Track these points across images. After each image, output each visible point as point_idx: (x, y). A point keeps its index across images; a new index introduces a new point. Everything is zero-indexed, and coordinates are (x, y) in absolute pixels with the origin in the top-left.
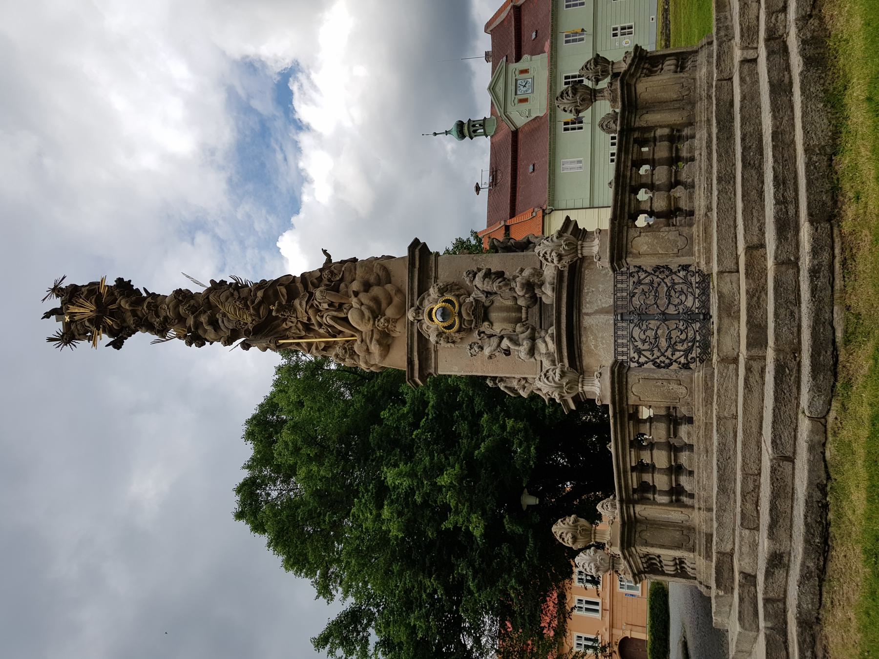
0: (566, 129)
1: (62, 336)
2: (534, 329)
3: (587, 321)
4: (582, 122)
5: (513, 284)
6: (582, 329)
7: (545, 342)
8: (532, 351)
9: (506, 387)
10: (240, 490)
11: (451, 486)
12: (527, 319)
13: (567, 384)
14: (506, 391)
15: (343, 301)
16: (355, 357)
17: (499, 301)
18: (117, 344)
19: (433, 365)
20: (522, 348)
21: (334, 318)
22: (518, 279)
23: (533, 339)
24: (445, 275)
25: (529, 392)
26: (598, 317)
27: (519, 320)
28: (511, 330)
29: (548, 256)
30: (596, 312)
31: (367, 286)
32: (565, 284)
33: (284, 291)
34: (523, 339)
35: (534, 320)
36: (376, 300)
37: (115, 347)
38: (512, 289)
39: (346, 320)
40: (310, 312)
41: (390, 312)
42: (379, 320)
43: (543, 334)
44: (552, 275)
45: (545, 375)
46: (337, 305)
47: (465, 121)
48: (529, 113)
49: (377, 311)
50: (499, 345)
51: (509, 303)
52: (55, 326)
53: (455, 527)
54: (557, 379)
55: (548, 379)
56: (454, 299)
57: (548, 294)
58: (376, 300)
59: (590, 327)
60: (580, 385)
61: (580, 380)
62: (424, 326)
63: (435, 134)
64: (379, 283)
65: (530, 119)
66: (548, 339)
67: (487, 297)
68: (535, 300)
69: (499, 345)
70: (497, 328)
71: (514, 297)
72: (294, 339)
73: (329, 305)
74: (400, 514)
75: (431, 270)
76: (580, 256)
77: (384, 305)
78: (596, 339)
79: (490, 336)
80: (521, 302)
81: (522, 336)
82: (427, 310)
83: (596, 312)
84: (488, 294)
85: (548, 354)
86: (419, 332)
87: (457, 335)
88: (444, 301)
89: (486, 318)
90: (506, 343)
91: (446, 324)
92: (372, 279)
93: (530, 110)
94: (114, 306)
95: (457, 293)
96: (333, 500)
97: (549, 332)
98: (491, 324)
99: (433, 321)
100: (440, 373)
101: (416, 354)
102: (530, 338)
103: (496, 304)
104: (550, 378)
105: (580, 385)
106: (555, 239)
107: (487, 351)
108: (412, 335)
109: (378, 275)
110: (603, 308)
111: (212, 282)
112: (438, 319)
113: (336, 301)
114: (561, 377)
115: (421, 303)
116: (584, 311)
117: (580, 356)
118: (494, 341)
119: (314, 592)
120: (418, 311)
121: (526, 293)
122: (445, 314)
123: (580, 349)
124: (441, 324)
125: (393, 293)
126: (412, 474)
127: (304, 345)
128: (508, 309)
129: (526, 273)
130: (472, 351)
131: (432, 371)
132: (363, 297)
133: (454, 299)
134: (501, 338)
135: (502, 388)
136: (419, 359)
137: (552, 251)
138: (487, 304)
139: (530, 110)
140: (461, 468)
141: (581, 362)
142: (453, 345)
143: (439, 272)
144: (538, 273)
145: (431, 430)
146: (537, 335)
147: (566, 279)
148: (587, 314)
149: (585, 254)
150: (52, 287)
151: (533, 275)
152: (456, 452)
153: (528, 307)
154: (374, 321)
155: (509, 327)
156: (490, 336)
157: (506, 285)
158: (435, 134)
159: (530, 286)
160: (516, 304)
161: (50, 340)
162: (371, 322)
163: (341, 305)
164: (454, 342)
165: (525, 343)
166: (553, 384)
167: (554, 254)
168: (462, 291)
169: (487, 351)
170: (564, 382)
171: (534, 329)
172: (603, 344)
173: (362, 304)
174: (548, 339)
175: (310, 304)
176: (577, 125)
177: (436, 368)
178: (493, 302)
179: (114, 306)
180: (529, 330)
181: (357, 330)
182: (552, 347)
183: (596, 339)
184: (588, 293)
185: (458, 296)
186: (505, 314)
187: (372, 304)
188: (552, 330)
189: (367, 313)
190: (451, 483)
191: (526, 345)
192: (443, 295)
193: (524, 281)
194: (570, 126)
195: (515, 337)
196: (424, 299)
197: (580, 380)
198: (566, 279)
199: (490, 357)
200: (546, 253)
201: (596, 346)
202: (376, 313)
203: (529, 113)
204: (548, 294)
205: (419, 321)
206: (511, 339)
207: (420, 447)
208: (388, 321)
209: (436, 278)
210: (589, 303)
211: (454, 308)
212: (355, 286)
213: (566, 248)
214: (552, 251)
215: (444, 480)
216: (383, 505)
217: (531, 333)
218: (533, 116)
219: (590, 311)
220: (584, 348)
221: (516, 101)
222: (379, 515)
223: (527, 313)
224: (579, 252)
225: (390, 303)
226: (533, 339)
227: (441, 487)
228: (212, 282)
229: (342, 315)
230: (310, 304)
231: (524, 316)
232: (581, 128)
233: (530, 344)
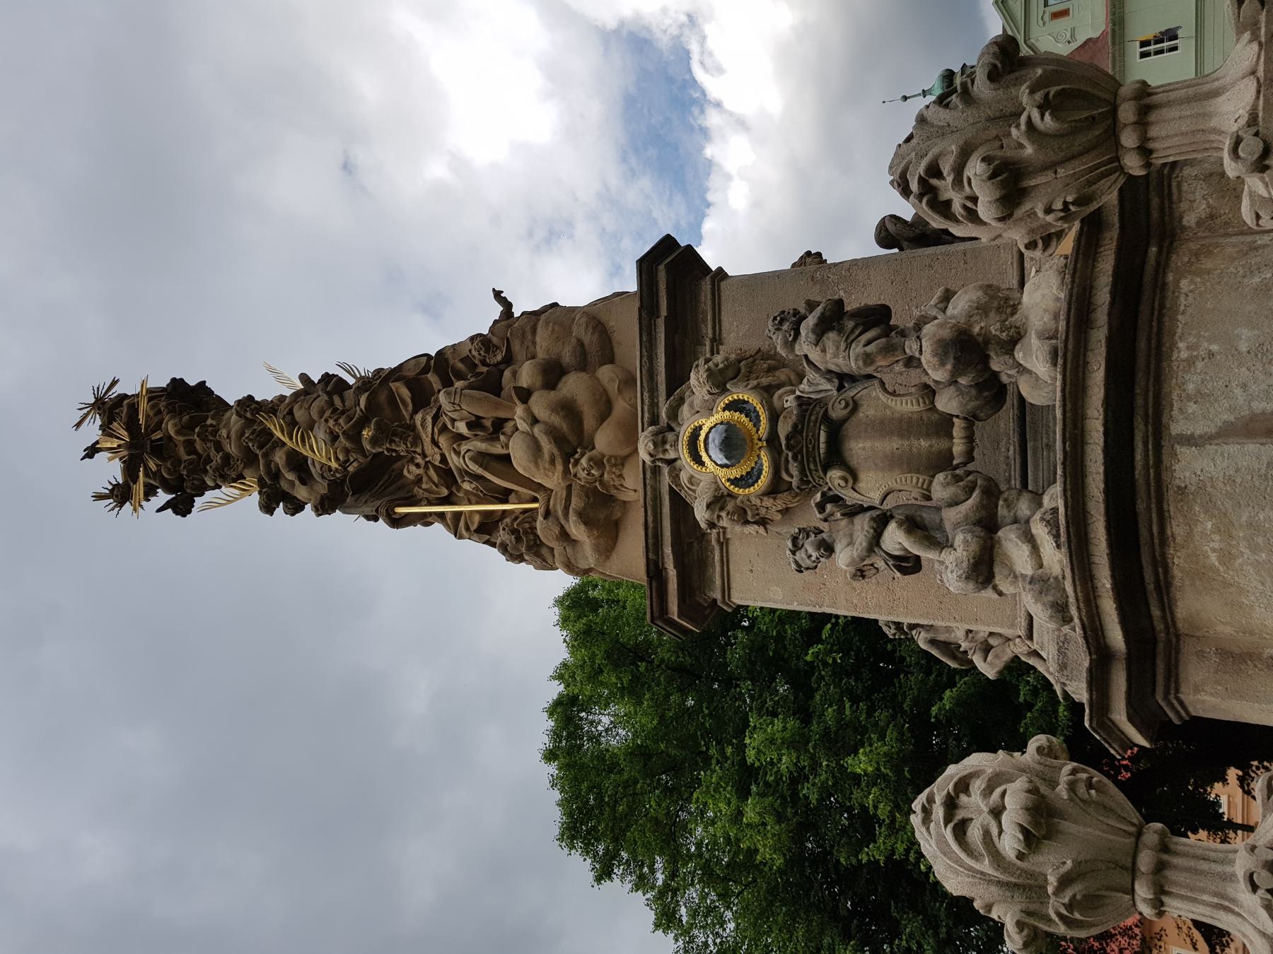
0: (1144, 55)
1: (112, 491)
2: (992, 493)
3: (1189, 466)
4: (1176, 38)
5: (911, 347)
6: (1170, 495)
7: (1030, 539)
8: (983, 569)
9: (933, 642)
10: (552, 711)
11: (876, 778)
12: (969, 457)
13: (1065, 882)
14: (935, 652)
15: (502, 415)
16: (544, 551)
17: (874, 403)
18: (182, 506)
19: (718, 582)
20: (948, 557)
21: (481, 458)
22: (928, 329)
23: (987, 525)
24: (740, 332)
25: (1000, 665)
26: (1232, 448)
27: (942, 462)
28: (916, 493)
29: (947, 191)
30: (1227, 433)
31: (553, 374)
32: (1099, 335)
33: (405, 393)
34: (956, 526)
35: (998, 455)
36: (569, 409)
37: (176, 513)
38: (912, 362)
39: (506, 459)
40: (443, 441)
41: (604, 440)
42: (577, 462)
43: (1023, 507)
44: (1051, 305)
45: (951, 804)
46: (488, 423)
47: (957, 69)
48: (1073, 36)
49: (572, 438)
50: (875, 542)
51: (908, 406)
52: (109, 469)
53: (889, 858)
54: (1009, 844)
55: (960, 831)
56: (754, 400)
57: (1036, 373)
58: (569, 409)
59: (1201, 487)
60: (1143, 891)
61: (1145, 861)
62: (684, 477)
63: (905, 98)
64: (583, 364)
65: (1075, 45)
66: (1040, 531)
67: (840, 388)
68: (993, 392)
69: (875, 542)
70: (872, 488)
71: (926, 386)
72: (430, 504)
73: (470, 426)
74: (780, 818)
75: (704, 320)
76: (1133, 164)
77: (589, 421)
78: (1225, 530)
79: (853, 512)
80: (947, 403)
81: (951, 516)
82: (685, 432)
83: (1227, 433)
84: (843, 379)
85: (1041, 583)
86: (672, 492)
87: (768, 502)
88: (728, 407)
89: (836, 456)
90: (895, 539)
91: (735, 473)
92: (567, 358)
93: (1073, 30)
94: (157, 435)
95: (765, 381)
96: (670, 762)
97: (1047, 502)
98: (853, 475)
99: (702, 464)
100: (737, 599)
101: (668, 550)
102: (978, 523)
103: (868, 411)
104: (974, 833)
105: (1143, 891)
106: (982, 87)
107: (843, 557)
108: (657, 499)
109: (581, 343)
110: (1254, 418)
111: (304, 378)
112: (714, 456)
113: (488, 414)
114: (1032, 839)
115: (674, 414)
116: (1178, 427)
117: (1165, 587)
118: (862, 525)
119: (651, 916)
120: (663, 436)
121: (956, 373)
122: (733, 444)
123: (1162, 565)
124: (721, 473)
125: (613, 388)
126: (797, 743)
127: (448, 517)
128: (903, 427)
129: (960, 306)
130: (800, 555)
131: (717, 595)
132: (540, 404)
133: (754, 400)
134: (882, 521)
135: (923, 646)
136: (678, 564)
137: (965, 154)
138: (837, 412)
139: (1073, 30)
140: (901, 739)
141: (1167, 605)
142: (761, 530)
143: (725, 325)
144: (1002, 302)
145: (845, 649)
146: (1002, 511)
147: (1101, 317)
148: (1189, 440)
149: (1165, 152)
150: (92, 400)
151: (982, 309)
152: (895, 695)
153: (971, 420)
154: (566, 463)
155: (907, 489)
156: (853, 512)
157: (889, 350)
158: (905, 98)
159: (968, 350)
160: (933, 409)
161: (99, 497)
162: (560, 467)
163: (499, 424)
164: (763, 522)
165: (959, 539)
166: (985, 866)
167: (975, 168)
168: (782, 375)
169: (843, 557)
170: (1052, 865)
171: (992, 493)
172: (1255, 549)
173: (535, 421)
174: (1040, 531)
175: (439, 425)
176: (1166, 45)
177: (726, 588)
178: (854, 406)
179: (157, 435)
180: (976, 493)
181: (540, 487)
182: (1055, 559)
183: (1225, 530)
184: (1191, 362)
185: (767, 391)
186: (893, 444)
187: (556, 420)
188: (1054, 497)
189: (547, 445)
190: (878, 769)
191: (962, 547)
192: (724, 390)
193: (946, 333)
194: (1152, 48)
195: (928, 517)
196: (681, 400)
197: (1145, 861)
198: (1101, 317)
199: (860, 574)
200: (934, 170)
201: (1227, 557)
202: (570, 442)
203: (1073, 36)
204: (1036, 373)
205: (671, 462)
206: (913, 525)
207: (823, 677)
208: (598, 463)
209: (717, 341)
210: (1199, 397)
211: (757, 424)
212: (526, 374)
213: (1047, 123)
214: (965, 154)
215: (861, 763)
216: (749, 793)
217: (981, 506)
218: (1081, 40)
219: (1200, 428)
220: (1179, 561)
221: (1047, 17)
222: (740, 813)
223: (970, 438)
224: (1129, 139)
225: (604, 416)
226: (987, 525)
227: (856, 779)
228: (304, 378)
229: (497, 449)
230: (439, 425)
231: (958, 447)
232: (1175, 48)
233: (974, 547)
